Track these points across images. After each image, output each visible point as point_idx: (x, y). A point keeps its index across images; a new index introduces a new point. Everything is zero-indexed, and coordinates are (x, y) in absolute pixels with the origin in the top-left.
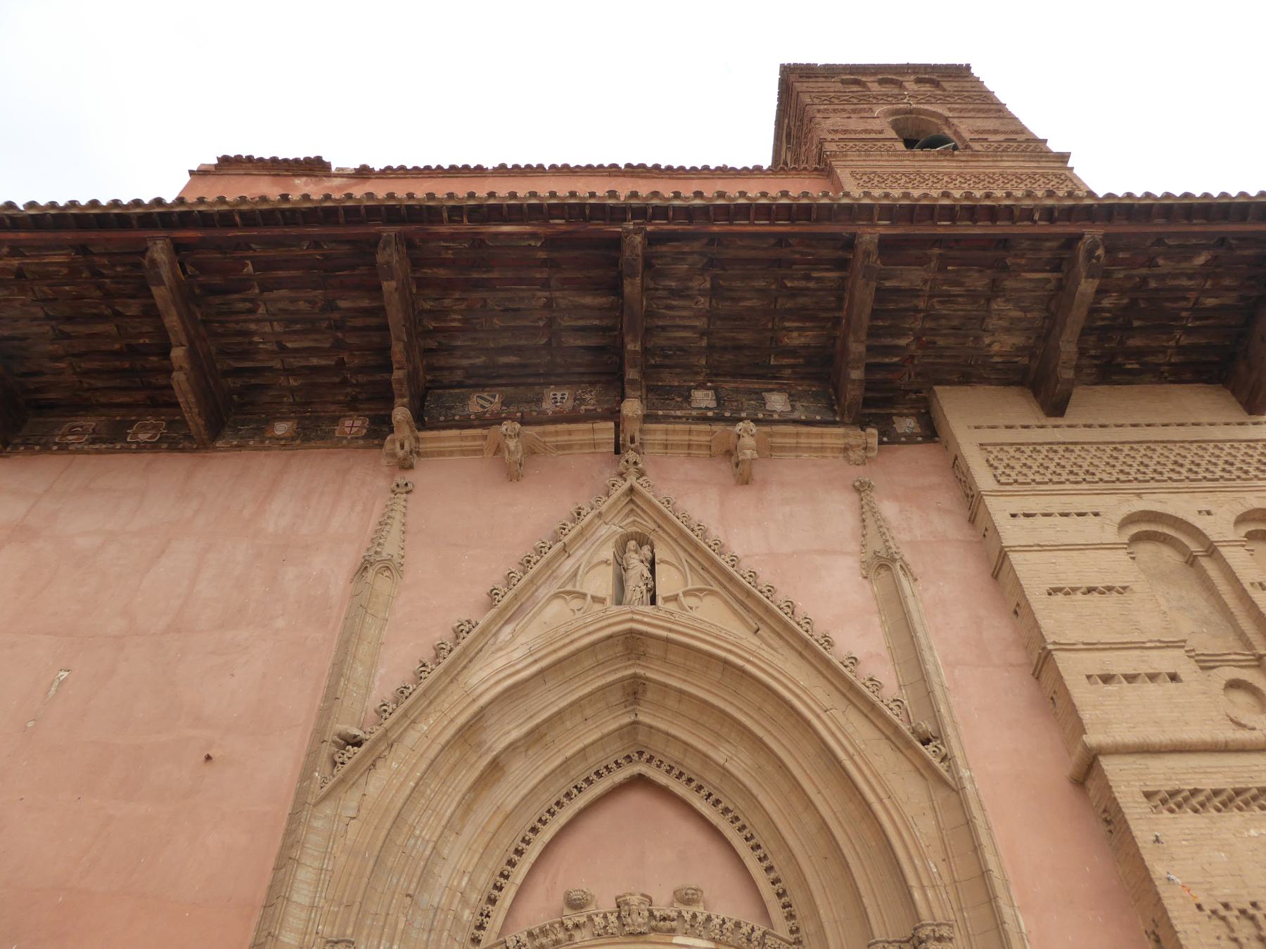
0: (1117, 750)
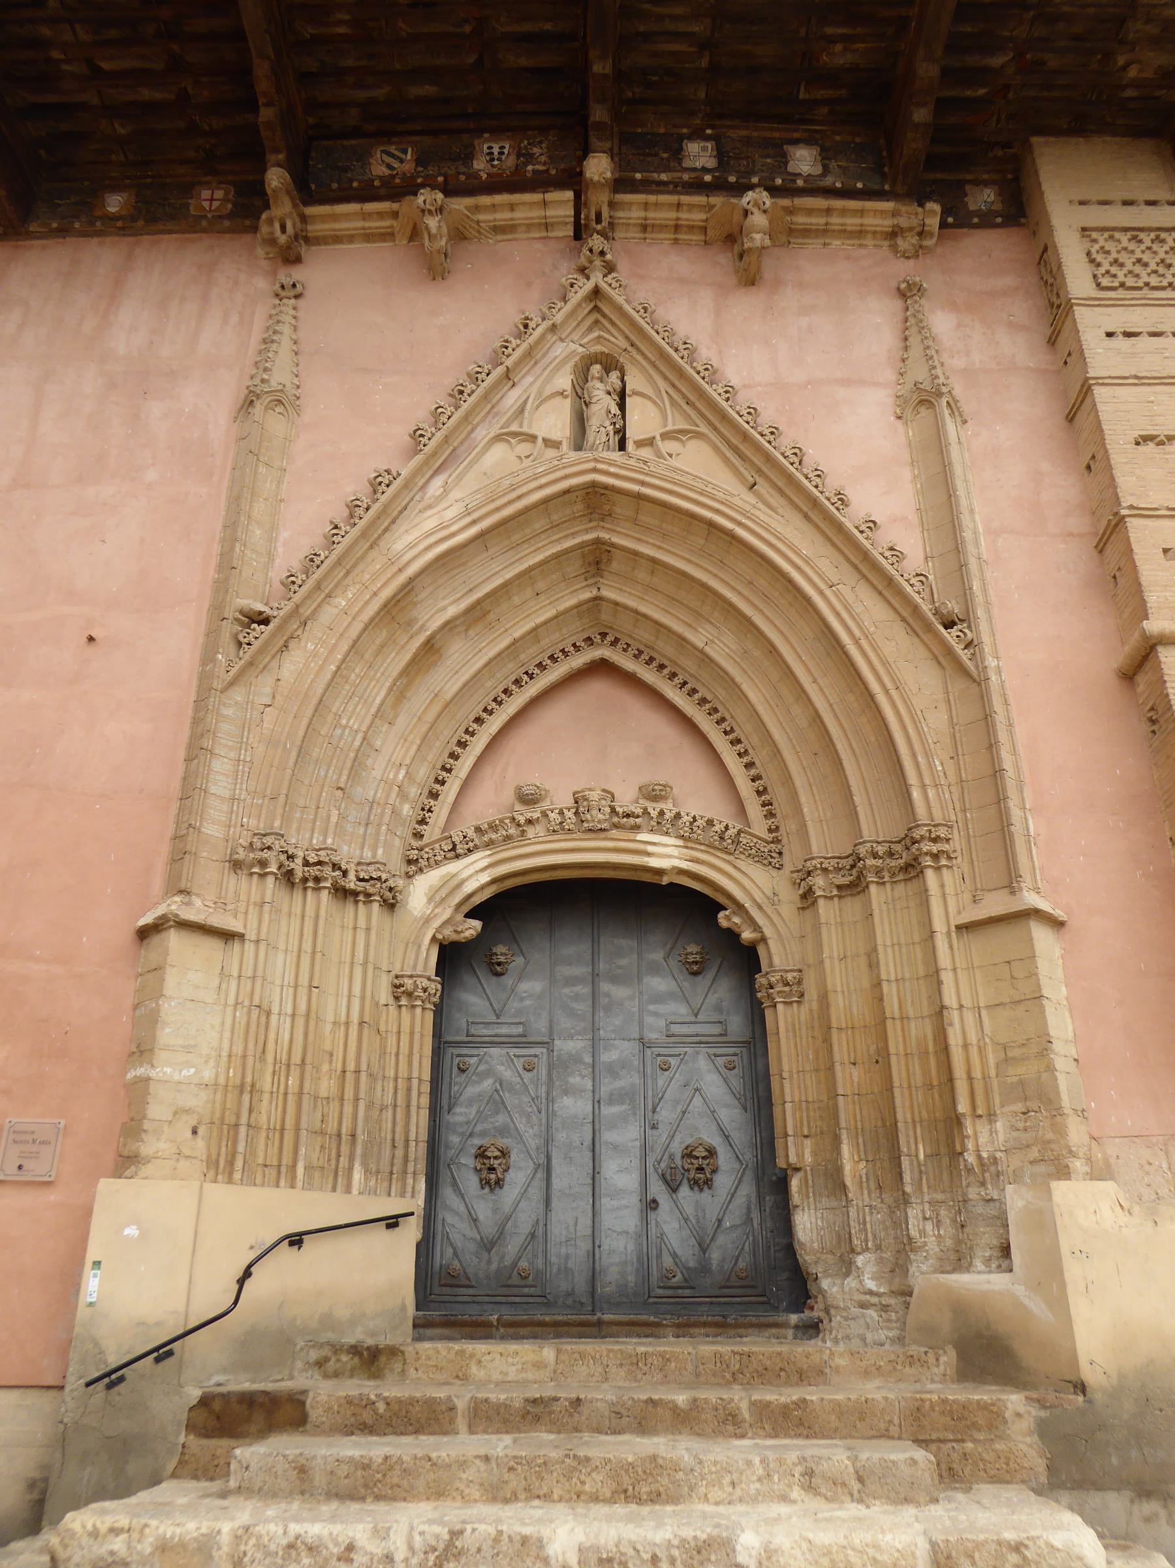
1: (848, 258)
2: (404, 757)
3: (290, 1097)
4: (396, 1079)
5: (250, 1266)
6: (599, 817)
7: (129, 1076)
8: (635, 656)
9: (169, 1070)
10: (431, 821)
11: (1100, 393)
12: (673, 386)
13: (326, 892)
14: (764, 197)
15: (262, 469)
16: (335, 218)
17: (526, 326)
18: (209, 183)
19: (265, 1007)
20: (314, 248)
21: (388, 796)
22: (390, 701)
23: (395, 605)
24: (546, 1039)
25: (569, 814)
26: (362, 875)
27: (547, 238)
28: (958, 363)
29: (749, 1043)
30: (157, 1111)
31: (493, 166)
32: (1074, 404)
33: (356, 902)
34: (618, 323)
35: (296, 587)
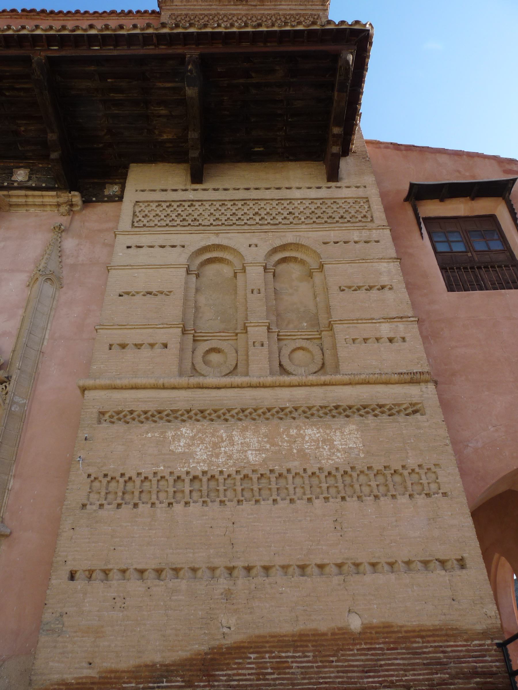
0: (102, 387)
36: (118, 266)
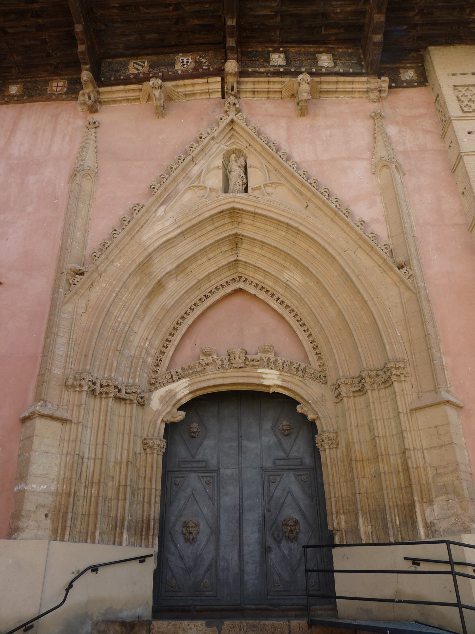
1: (347, 103)
2: (148, 336)
3: (93, 498)
4: (144, 489)
5: (72, 582)
6: (239, 362)
7: (15, 489)
8: (255, 286)
9: (34, 486)
10: (161, 365)
11: (466, 158)
12: (269, 162)
13: (111, 399)
14: (307, 77)
15: (81, 205)
16: (113, 92)
17: (201, 138)
18: (55, 79)
19: (81, 455)
20: (103, 106)
21: (141, 354)
22: (141, 310)
23: (143, 265)
24: (216, 469)
25: (226, 361)
26: (128, 391)
27: (209, 98)
28: (400, 148)
29: (313, 469)
30: (29, 506)
31: (184, 67)
32: (455, 165)
33: (126, 404)
34: (243, 135)
35: (96, 258)
36: (471, 152)
